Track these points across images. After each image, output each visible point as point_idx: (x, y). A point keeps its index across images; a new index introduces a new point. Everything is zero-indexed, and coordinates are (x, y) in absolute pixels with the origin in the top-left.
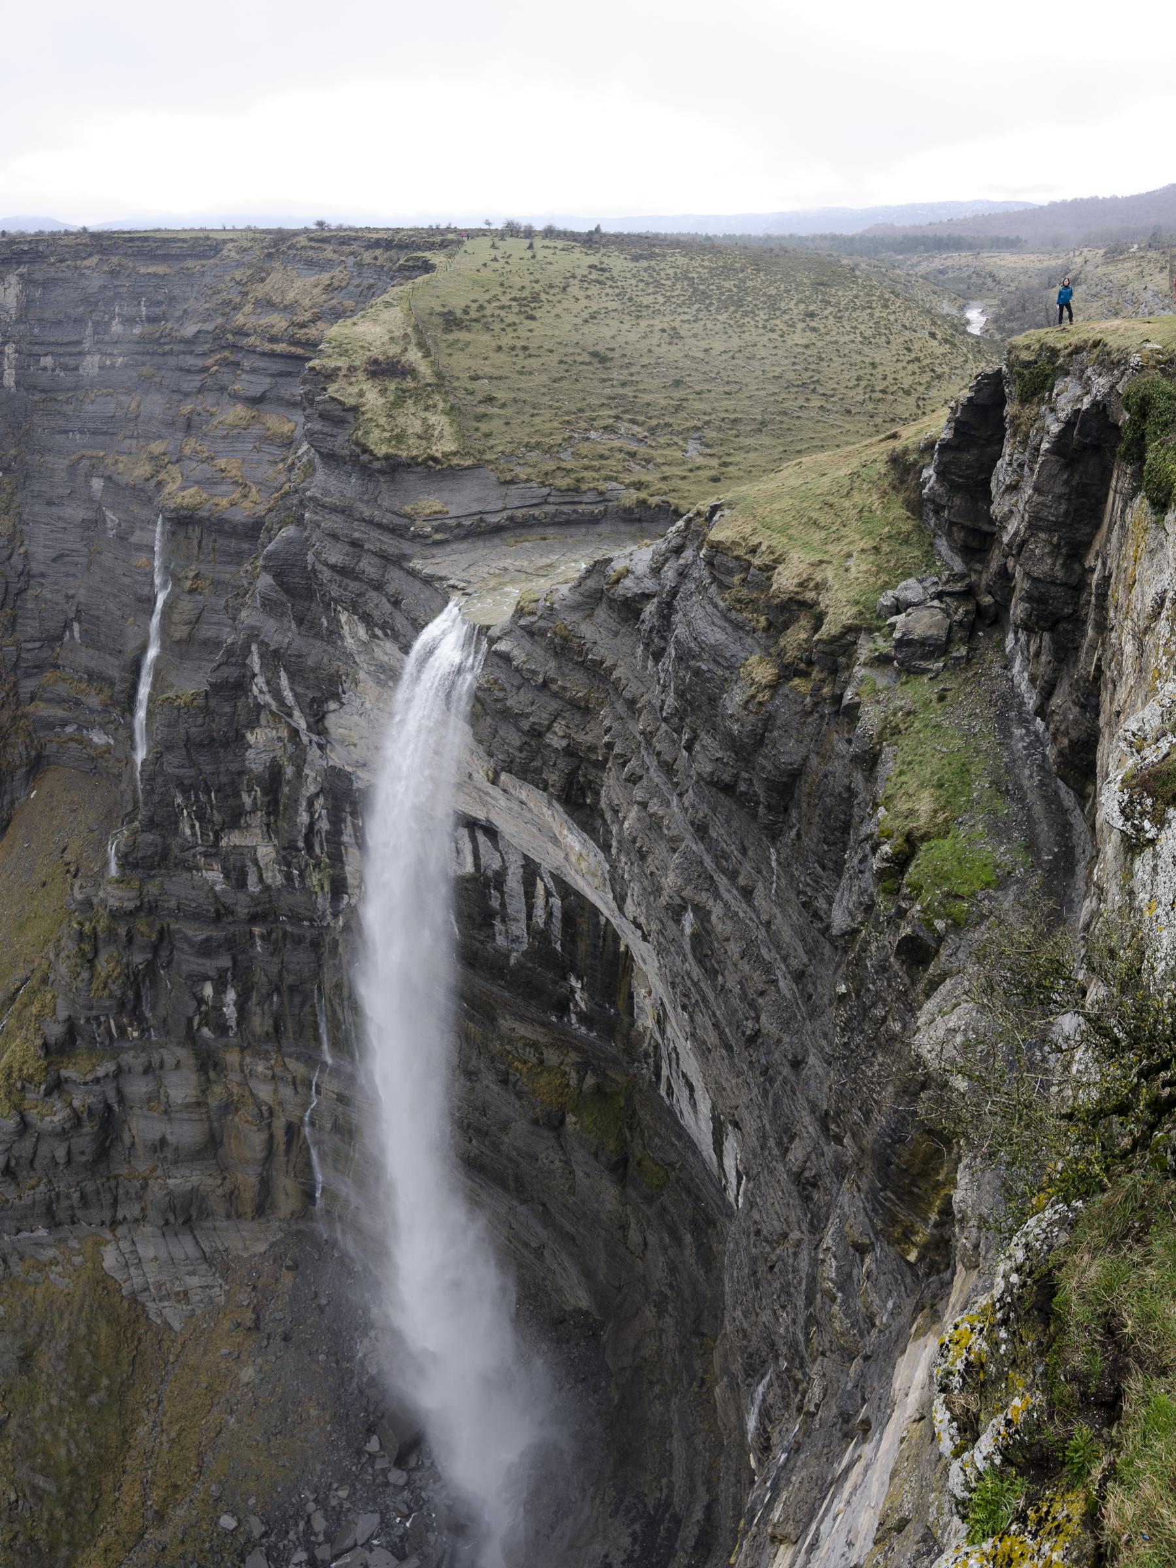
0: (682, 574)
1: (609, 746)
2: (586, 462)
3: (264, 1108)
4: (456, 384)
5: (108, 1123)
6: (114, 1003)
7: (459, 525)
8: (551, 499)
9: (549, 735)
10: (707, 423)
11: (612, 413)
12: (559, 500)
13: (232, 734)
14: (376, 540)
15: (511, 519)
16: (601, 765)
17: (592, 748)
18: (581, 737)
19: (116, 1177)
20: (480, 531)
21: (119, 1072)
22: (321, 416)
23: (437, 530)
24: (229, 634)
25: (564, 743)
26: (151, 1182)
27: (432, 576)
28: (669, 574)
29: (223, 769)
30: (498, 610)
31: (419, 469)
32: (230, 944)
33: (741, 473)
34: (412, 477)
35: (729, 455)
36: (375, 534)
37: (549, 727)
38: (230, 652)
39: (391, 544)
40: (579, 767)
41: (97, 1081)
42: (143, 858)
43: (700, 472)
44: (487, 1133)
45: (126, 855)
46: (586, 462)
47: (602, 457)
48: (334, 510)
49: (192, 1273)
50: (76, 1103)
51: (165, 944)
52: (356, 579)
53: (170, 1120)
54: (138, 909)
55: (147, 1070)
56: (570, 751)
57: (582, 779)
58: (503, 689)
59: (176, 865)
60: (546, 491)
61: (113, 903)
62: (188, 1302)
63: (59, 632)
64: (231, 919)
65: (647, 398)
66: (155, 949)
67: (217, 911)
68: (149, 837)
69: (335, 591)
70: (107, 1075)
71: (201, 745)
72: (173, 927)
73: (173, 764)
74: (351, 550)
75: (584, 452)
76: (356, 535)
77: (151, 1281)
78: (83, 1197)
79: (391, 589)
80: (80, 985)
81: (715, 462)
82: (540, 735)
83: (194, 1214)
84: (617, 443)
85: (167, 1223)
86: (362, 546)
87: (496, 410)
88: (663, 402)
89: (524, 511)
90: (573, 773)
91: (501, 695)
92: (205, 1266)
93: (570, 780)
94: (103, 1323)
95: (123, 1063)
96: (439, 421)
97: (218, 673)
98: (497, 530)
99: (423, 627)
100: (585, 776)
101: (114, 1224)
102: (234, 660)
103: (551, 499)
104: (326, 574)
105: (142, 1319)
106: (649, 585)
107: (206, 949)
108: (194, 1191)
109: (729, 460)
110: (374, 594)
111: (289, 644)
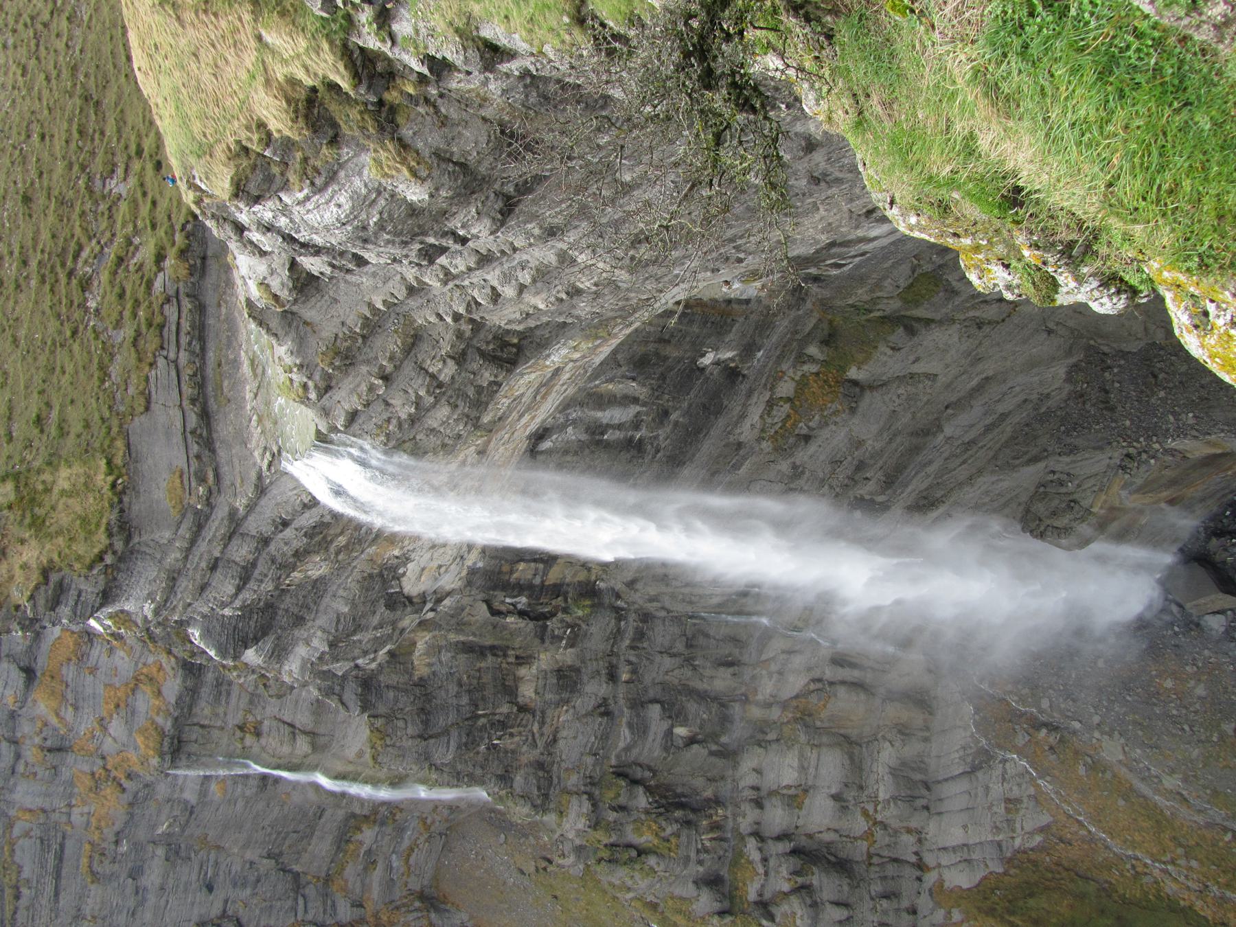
0: (268, 228)
1: (457, 317)
2: (127, 314)
3: (812, 687)
4: (17, 459)
5: (809, 855)
6: (685, 832)
7: (198, 457)
8: (172, 356)
9: (441, 378)
10: (83, 168)
11: (63, 277)
12: (173, 348)
13: (417, 691)
14: (207, 548)
15: (193, 401)
16: (477, 326)
17: (459, 335)
18: (446, 348)
19: (870, 856)
20: (204, 433)
21: (757, 835)
22: (53, 609)
23: (202, 480)
24: (309, 692)
25: (450, 363)
26: (879, 817)
27: (256, 486)
28: (265, 241)
29: (455, 702)
30: (301, 420)
31: (126, 499)
32: (638, 704)
33: (152, 135)
34: (135, 508)
35: (126, 147)
36: (202, 546)
37: (433, 376)
38: (329, 692)
39: (217, 525)
40: (478, 349)
41: (765, 860)
42: (539, 788)
43: (148, 185)
44: (861, 462)
45: (534, 806)
46: (127, 314)
47: (121, 296)
48: (171, 589)
49: (987, 789)
50: (786, 887)
51: (630, 771)
52: (254, 564)
53: (814, 787)
54: (591, 797)
55: (758, 804)
56: (460, 358)
57: (491, 347)
58: (389, 420)
59: (550, 754)
60: (161, 362)
61: (581, 824)
62: (1018, 801)
63: (289, 877)
64: (611, 701)
65: (45, 235)
66: (635, 782)
67: (602, 715)
68: (519, 780)
69: (268, 586)
70: (760, 849)
71: (426, 723)
72: (613, 762)
73: (444, 753)
74: (219, 570)
75: (115, 316)
76: (203, 565)
77: (990, 838)
78: (886, 896)
79: (267, 530)
80: (662, 867)
81: (136, 166)
82: (440, 385)
83: (918, 777)
84: (105, 276)
85: (927, 808)
86: (217, 559)
87: (54, 414)
88: (51, 218)
89: (184, 387)
90: (482, 354)
91: (394, 421)
92: (980, 774)
93: (492, 358)
94: (1032, 902)
95: (749, 830)
96: (64, 478)
97: (351, 705)
98: (205, 416)
99: (314, 498)
100: (488, 343)
101: (921, 866)
102: (337, 688)
103: (172, 356)
104: (247, 596)
105: (1033, 856)
106: (280, 261)
107: (640, 729)
108: (894, 772)
109: (133, 148)
110: (272, 547)
111: (324, 631)
